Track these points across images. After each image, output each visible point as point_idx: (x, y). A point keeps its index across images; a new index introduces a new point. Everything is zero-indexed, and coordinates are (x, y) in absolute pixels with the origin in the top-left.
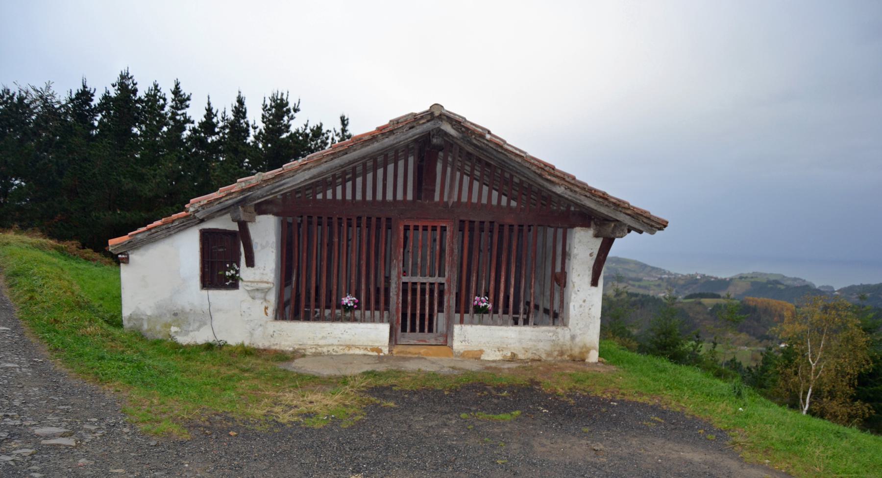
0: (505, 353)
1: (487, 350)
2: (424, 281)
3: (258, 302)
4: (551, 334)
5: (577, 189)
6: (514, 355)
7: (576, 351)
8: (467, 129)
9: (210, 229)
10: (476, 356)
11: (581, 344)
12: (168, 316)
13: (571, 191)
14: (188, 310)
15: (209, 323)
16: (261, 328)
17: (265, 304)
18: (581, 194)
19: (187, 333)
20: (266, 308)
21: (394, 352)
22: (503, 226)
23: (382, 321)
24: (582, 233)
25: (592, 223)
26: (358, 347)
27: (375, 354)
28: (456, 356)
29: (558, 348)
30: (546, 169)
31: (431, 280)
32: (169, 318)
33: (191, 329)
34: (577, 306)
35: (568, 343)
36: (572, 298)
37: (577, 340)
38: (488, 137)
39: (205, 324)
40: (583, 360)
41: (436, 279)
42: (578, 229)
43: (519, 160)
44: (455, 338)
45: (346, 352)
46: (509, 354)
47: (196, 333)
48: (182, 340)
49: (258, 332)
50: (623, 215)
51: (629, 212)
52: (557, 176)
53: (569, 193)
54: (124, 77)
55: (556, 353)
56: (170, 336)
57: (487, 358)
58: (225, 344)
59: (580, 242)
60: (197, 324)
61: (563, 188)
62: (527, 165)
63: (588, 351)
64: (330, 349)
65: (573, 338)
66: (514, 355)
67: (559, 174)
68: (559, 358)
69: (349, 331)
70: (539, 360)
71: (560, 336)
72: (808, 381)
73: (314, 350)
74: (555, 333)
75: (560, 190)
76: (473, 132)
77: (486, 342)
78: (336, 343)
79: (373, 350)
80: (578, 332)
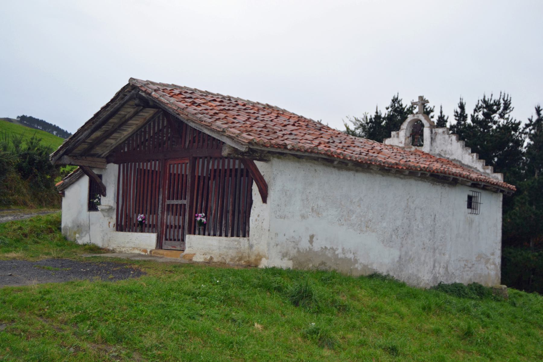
4: (236, 243)
7: (253, 258)
11: (256, 252)
20: (109, 223)
23: (153, 232)
29: (240, 255)
34: (254, 220)
35: (247, 251)
37: (254, 248)
40: (256, 266)
46: (209, 258)
48: (80, 242)
54: (395, 100)
65: (251, 247)
68: (238, 262)
71: (242, 244)
74: (239, 242)
77: (201, 247)
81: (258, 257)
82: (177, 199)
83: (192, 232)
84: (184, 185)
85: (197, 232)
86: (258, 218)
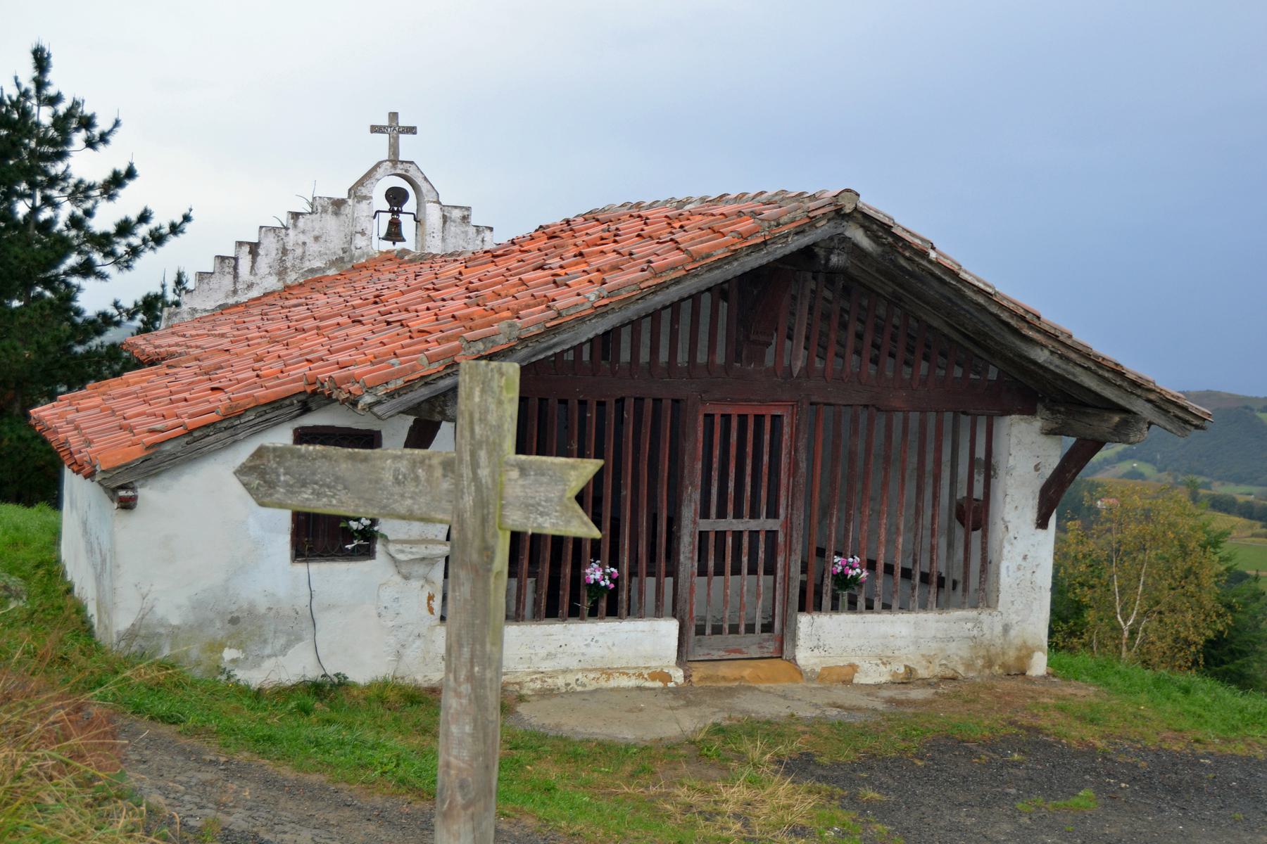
0: (894, 667)
1: (864, 665)
2: (741, 528)
3: (415, 584)
4: (970, 625)
5: (1073, 356)
6: (910, 670)
8: (898, 238)
9: (315, 427)
10: (845, 676)
11: (1018, 642)
12: (218, 625)
13: (1061, 356)
14: (262, 610)
15: (308, 637)
16: (418, 643)
17: (428, 589)
18: (1076, 364)
19: (257, 662)
20: (431, 598)
21: (694, 679)
22: (643, 399)
24: (1023, 424)
25: (1040, 406)
26: (623, 672)
27: (658, 684)
28: (809, 680)
29: (982, 653)
30: (1028, 319)
31: (753, 525)
32: (218, 630)
33: (268, 651)
34: (1013, 567)
35: (999, 642)
36: (1005, 551)
37: (1012, 633)
38: (933, 255)
39: (299, 639)
41: (763, 524)
42: (1015, 418)
43: (981, 300)
44: (800, 642)
45: (603, 684)
46: (902, 670)
47: (280, 658)
48: (254, 677)
49: (413, 653)
50: (1140, 402)
51: (1152, 397)
52: (1045, 333)
53: (1057, 361)
55: (980, 662)
56: (223, 671)
57: (870, 681)
58: (341, 684)
59: (1019, 443)
60: (282, 640)
61: (1046, 353)
62: (994, 309)
63: (1029, 656)
64: (571, 678)
65: (1006, 629)
66: (910, 670)
67: (1047, 328)
68: (987, 671)
69: (601, 639)
70: (954, 679)
71: (985, 627)
72: (669, 817)
73: (538, 685)
74: (977, 623)
75: (1042, 356)
76: (908, 245)
77: (860, 648)
78: (574, 664)
79: (653, 676)
80: (1014, 618)
81: (1024, 652)
82: (738, 515)
83: (810, 601)
84: (716, 461)
85: (827, 601)
86: (1024, 564)
